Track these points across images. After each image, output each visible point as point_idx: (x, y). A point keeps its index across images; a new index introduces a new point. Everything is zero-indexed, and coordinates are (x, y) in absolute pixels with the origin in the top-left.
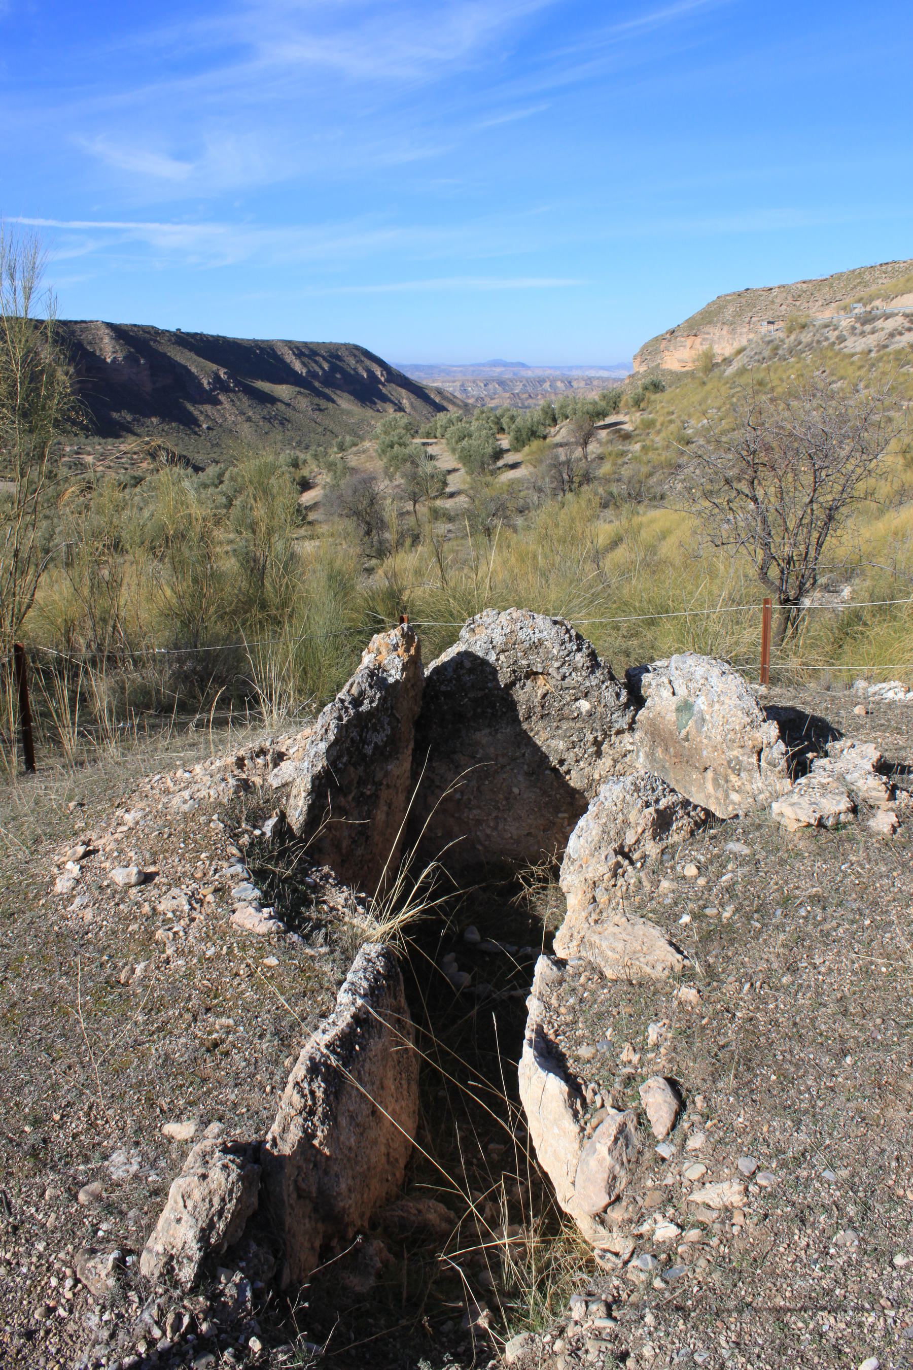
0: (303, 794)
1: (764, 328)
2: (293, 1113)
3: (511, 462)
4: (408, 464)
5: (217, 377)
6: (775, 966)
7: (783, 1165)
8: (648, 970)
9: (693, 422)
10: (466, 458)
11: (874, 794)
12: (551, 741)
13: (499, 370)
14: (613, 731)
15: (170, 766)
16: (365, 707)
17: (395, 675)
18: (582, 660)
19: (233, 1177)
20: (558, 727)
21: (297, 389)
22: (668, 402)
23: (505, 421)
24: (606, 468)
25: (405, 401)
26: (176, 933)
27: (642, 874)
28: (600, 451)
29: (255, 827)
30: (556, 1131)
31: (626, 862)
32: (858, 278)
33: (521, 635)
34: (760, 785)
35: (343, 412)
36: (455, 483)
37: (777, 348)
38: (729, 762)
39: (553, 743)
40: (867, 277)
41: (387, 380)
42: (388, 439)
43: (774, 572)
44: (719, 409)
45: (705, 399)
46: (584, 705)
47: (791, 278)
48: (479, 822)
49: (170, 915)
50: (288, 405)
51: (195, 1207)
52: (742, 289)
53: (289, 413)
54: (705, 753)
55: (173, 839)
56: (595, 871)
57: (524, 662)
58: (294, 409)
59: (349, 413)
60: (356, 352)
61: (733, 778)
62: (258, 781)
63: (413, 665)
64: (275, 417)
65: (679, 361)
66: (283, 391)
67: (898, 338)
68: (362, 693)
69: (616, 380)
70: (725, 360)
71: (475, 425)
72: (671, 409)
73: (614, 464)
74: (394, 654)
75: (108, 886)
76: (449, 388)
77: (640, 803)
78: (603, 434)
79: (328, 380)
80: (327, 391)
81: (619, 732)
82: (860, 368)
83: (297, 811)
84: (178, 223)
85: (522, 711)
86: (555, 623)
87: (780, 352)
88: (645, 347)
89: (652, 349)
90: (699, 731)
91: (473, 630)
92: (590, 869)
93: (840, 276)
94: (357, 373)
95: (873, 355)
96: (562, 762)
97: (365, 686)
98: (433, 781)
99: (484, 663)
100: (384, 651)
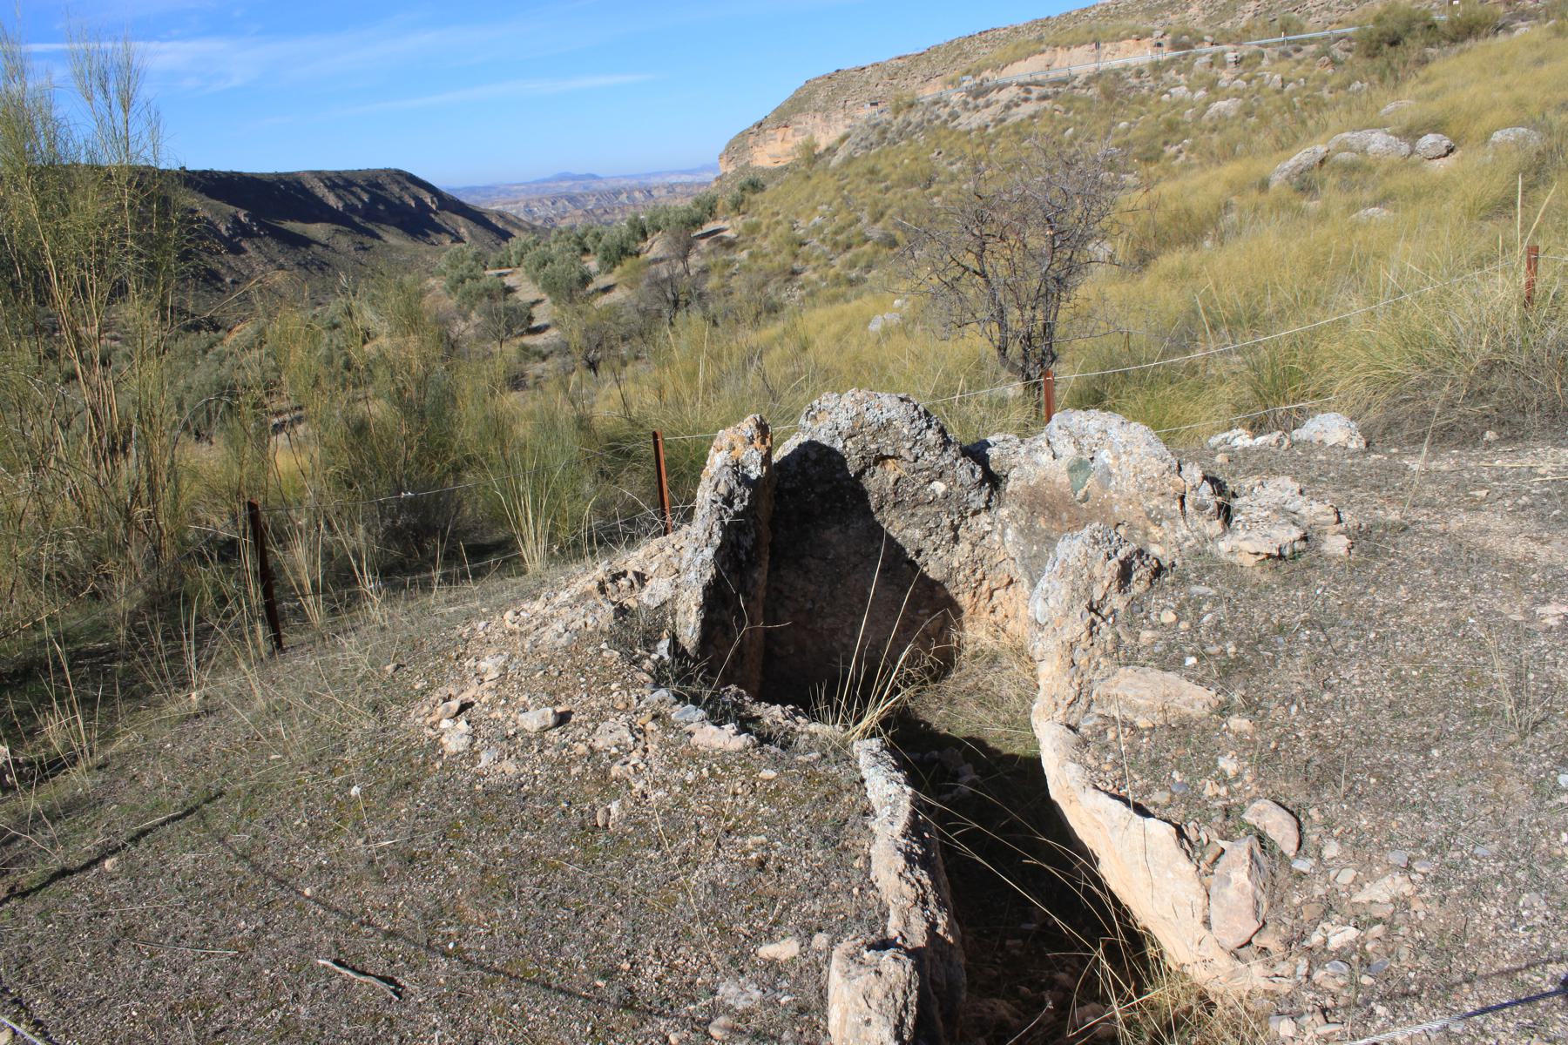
0: (695, 609)
1: (866, 112)
2: (909, 904)
3: (602, 286)
4: (486, 299)
5: (236, 220)
6: (1309, 686)
7: (1433, 851)
8: (1188, 710)
9: (802, 222)
10: (551, 287)
11: (1322, 518)
12: (903, 529)
13: (566, 184)
14: (970, 512)
15: (501, 608)
16: (738, 506)
17: (755, 472)
18: (934, 438)
19: (909, 967)
20: (913, 515)
21: (335, 227)
22: (771, 202)
23: (588, 241)
24: (713, 282)
25: (462, 230)
26: (635, 766)
27: (1118, 629)
28: (702, 263)
29: (650, 652)
30: (1170, 875)
31: (1099, 619)
32: (956, 50)
33: (869, 417)
34: (1185, 532)
35: (392, 248)
36: (541, 316)
37: (884, 132)
38: (1148, 514)
39: (908, 532)
40: (967, 47)
41: (441, 208)
42: (457, 274)
43: (1015, 350)
44: (830, 204)
45: (811, 196)
46: (939, 487)
47: (885, 53)
48: (833, 632)
49: (614, 750)
50: (326, 246)
51: (880, 1005)
52: (832, 71)
53: (328, 256)
54: (1116, 509)
55: (564, 675)
56: (1073, 631)
57: (873, 446)
58: (334, 250)
59: (398, 249)
60: (400, 178)
61: (1153, 530)
62: (632, 603)
63: (766, 460)
64: (312, 262)
65: (771, 156)
66: (318, 231)
67: (1015, 110)
68: (731, 492)
69: (700, 185)
70: (828, 149)
71: (555, 249)
72: (776, 209)
73: (721, 276)
74: (752, 448)
75: (515, 735)
76: (512, 210)
77: (1103, 556)
78: (704, 243)
79: (370, 213)
80: (370, 226)
81: (976, 513)
82: (978, 145)
83: (689, 628)
84: (168, 40)
85: (873, 501)
86: (902, 400)
87: (889, 135)
88: (731, 144)
89: (739, 146)
90: (1104, 487)
91: (815, 417)
92: (1067, 630)
93: (936, 49)
94: (403, 202)
95: (991, 130)
96: (918, 553)
97: (733, 483)
98: (781, 592)
99: (831, 451)
100: (739, 446)
